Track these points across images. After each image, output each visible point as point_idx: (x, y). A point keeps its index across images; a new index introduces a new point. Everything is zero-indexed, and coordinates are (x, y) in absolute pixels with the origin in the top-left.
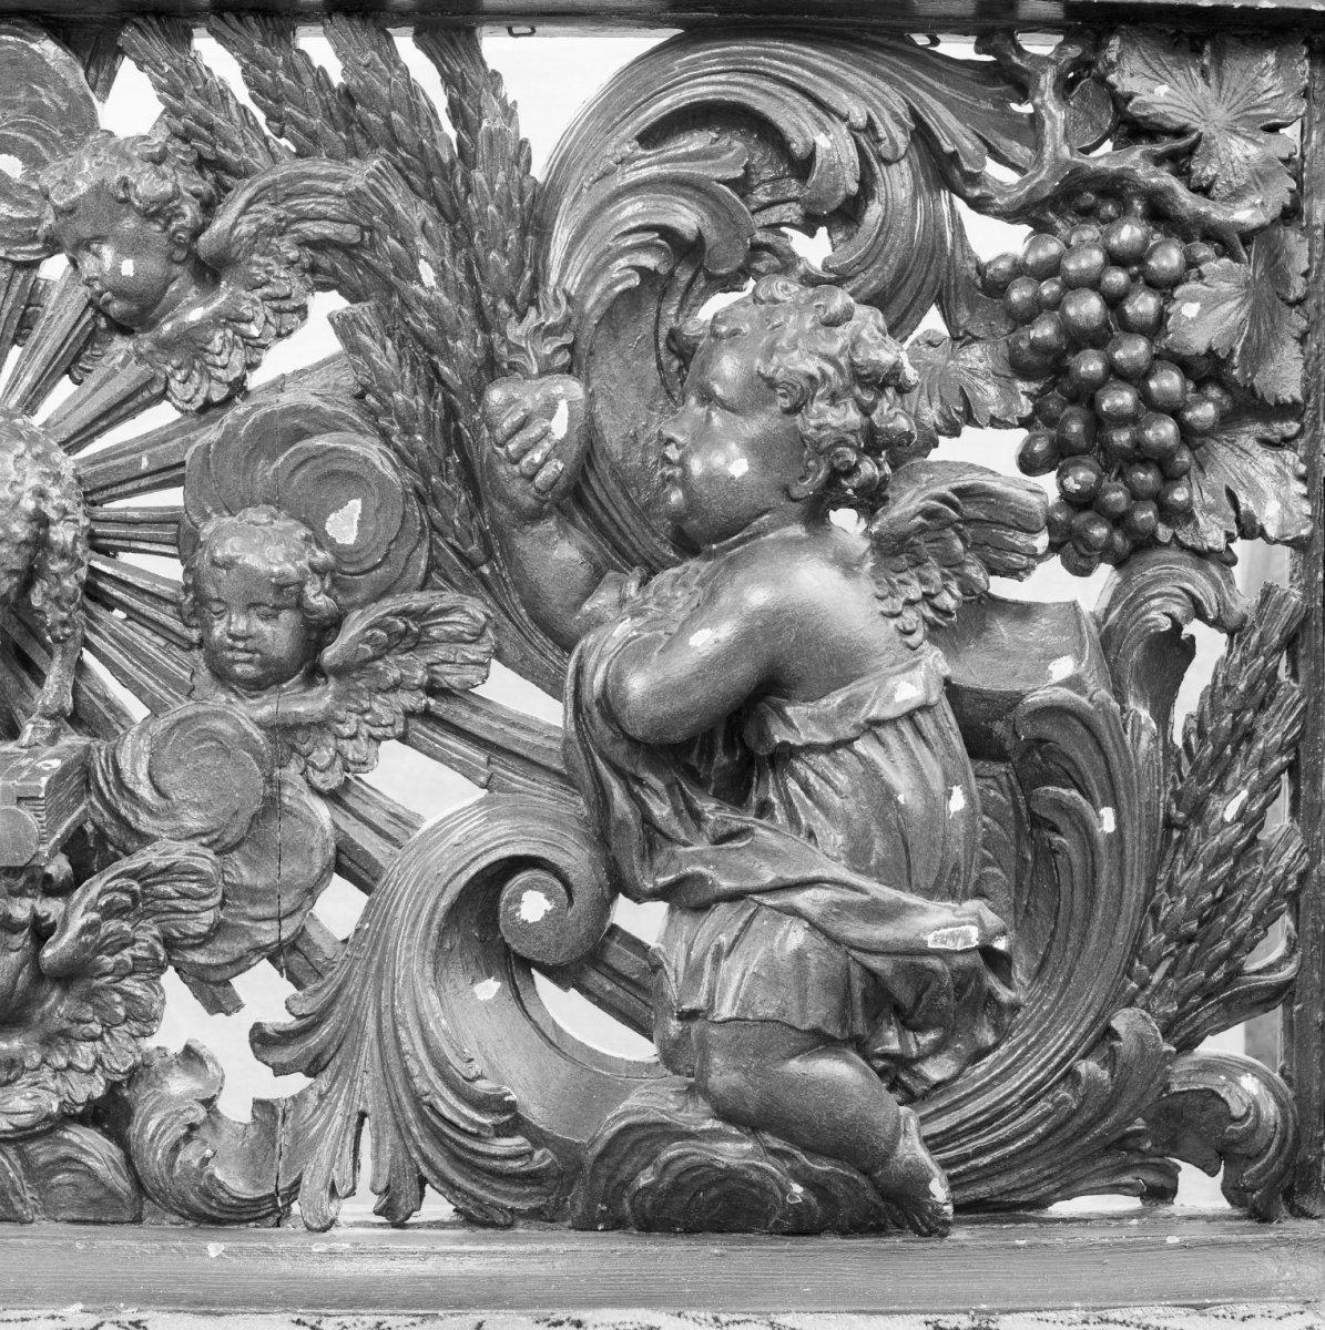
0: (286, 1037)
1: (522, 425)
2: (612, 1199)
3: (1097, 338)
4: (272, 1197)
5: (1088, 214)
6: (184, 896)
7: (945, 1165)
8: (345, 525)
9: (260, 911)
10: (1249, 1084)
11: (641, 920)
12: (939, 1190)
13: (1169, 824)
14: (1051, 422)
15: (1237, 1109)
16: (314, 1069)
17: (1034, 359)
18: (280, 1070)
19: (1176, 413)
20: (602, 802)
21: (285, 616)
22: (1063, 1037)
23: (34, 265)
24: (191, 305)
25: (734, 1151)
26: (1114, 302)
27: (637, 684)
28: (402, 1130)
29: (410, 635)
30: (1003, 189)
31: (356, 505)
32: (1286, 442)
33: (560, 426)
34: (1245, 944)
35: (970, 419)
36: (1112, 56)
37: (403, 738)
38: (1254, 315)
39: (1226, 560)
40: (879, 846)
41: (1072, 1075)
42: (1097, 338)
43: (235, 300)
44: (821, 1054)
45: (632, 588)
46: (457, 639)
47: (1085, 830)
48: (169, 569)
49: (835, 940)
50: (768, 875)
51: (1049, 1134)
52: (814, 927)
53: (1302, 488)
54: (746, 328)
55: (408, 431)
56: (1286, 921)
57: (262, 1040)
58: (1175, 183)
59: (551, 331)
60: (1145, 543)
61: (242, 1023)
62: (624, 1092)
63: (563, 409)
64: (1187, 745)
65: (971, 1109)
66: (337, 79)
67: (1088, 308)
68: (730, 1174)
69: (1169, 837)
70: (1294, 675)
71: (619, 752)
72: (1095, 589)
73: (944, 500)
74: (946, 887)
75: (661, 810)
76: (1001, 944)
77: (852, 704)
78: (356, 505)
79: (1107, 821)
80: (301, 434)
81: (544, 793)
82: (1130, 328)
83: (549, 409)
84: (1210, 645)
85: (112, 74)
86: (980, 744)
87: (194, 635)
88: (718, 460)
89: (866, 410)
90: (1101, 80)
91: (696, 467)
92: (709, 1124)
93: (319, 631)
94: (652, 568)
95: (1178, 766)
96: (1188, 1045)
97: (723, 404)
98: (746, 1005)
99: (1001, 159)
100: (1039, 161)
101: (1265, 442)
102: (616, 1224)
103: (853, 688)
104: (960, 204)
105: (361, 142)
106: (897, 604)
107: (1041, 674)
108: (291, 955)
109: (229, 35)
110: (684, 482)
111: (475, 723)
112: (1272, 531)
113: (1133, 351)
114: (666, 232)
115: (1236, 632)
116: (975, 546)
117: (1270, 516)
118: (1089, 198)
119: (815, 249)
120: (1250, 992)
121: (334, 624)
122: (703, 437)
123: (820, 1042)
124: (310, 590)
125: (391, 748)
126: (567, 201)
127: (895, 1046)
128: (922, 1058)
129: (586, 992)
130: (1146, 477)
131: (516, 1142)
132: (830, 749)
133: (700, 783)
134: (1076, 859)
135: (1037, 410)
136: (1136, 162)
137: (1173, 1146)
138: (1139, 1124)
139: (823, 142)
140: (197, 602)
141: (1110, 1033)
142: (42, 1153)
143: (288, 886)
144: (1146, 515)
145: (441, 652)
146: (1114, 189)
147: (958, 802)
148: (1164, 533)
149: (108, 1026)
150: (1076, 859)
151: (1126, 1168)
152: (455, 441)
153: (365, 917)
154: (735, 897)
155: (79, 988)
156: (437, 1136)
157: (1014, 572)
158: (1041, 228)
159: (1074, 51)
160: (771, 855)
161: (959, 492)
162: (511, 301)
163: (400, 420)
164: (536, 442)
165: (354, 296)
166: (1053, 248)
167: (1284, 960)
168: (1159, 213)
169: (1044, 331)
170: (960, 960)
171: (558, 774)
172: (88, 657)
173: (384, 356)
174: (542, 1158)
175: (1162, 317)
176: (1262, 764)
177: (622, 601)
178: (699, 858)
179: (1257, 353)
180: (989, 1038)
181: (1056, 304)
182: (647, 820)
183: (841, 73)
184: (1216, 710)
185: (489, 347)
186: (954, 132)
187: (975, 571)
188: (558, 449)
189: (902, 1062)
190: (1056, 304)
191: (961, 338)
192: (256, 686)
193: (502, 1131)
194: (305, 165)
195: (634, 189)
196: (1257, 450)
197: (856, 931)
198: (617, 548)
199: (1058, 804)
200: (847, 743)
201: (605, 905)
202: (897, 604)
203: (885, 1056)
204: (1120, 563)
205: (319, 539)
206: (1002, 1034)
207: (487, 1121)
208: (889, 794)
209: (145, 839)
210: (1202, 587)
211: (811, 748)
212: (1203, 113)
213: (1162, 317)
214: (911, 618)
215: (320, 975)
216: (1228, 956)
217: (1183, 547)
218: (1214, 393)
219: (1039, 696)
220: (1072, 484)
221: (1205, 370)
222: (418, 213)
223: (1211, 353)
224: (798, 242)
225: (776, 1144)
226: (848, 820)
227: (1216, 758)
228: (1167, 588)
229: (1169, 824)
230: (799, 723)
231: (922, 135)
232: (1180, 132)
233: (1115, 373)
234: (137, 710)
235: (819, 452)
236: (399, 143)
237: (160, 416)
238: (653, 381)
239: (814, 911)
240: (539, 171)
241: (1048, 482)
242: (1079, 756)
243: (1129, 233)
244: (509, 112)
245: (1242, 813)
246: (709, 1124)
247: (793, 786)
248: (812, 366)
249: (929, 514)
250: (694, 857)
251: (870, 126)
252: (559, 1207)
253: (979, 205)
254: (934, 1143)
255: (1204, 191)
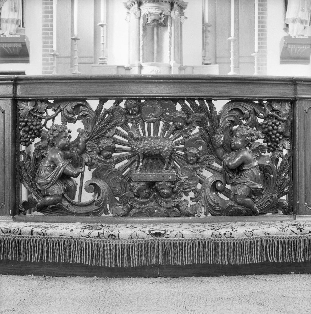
0: (194, 198)
1: (219, 139)
2: (227, 213)
3: (271, 131)
4: (194, 214)
5: (269, 118)
6: (185, 184)
7: (259, 209)
8: (200, 149)
9: (192, 186)
10: (285, 201)
11: (228, 187)
12: (258, 211)
13: (277, 177)
14: (266, 138)
15: (284, 204)
16: (197, 202)
17: (265, 132)
18: (193, 202)
19: (278, 138)
20: (226, 175)
21: (196, 157)
22: (268, 197)
23: (169, 123)
24: (186, 127)
25: (239, 208)
26: (273, 127)
27: (230, 164)
28: (207, 207)
29: (207, 159)
30: (262, 116)
31: (202, 146)
32: (288, 140)
33: (222, 139)
34: (284, 188)
35: (259, 138)
36: (272, 103)
37: (205, 169)
38: (285, 128)
39: (282, 151)
40: (253, 178)
41: (269, 201)
42: (271, 131)
43: (190, 127)
44: (248, 198)
45: (228, 154)
46: (212, 159)
47: (270, 177)
48: (183, 153)
49: (249, 187)
50: (243, 181)
51: (267, 206)
52: (247, 186)
53: (289, 144)
54: (240, 130)
55: (206, 139)
56: (288, 186)
57: (191, 199)
58: (278, 115)
59: (221, 130)
60: (275, 150)
61: (189, 197)
62: (228, 203)
63: (222, 137)
64: (279, 169)
65: (260, 204)
66: (199, 105)
67: (271, 128)
68: (239, 210)
69: (277, 178)
70: (289, 162)
71: (228, 170)
72: (270, 154)
73: (258, 146)
74: (259, 183)
75: (231, 176)
76: (263, 188)
77: (251, 165)
78: (202, 146)
79: (272, 176)
80: (196, 140)
81: (219, 174)
82: (274, 129)
83: (221, 137)
84: (281, 159)
85: (176, 104)
86: (261, 170)
87: (185, 159)
88: (237, 142)
89: (251, 138)
90: (271, 106)
91: (235, 143)
92: (237, 205)
93: (198, 159)
94: (229, 153)
95: (278, 171)
96: (279, 198)
97: (238, 137)
98: (241, 193)
99: (262, 113)
100: (265, 113)
101: (286, 140)
102: (227, 215)
103: (251, 164)
104: (257, 117)
105: (201, 111)
106: (253, 156)
107: (266, 162)
108: (195, 191)
109: (190, 101)
110: (234, 144)
111: (213, 168)
112: (287, 149)
113: (275, 132)
114: (231, 120)
115: (283, 158)
116: (261, 150)
117: (287, 147)
118: (270, 117)
119: (244, 122)
120: (285, 193)
121: (199, 158)
122: (236, 140)
123: (248, 197)
124: (198, 155)
125: (204, 170)
126: (221, 117)
127: (254, 198)
128: (255, 199)
129: (223, 194)
130: (275, 143)
131: (218, 208)
132: (248, 169)
133: (234, 173)
134: (269, 180)
135: (265, 137)
136: (274, 113)
137: (278, 208)
138: (275, 205)
139: (246, 112)
140: (186, 156)
141: (272, 197)
142: (171, 210)
143: (195, 184)
144: (275, 147)
145: (210, 161)
146: (272, 116)
147: (259, 175)
148: (277, 149)
149: (178, 197)
150: (269, 180)
151: (273, 210)
152: (210, 140)
153: (202, 187)
154: (239, 184)
155: (176, 194)
156: (211, 207)
157: (264, 153)
158: (265, 120)
159: (268, 103)
160: (243, 179)
161: (260, 145)
162: (216, 127)
163: (206, 138)
164: (220, 141)
165: (200, 126)
166: (267, 122)
167: (288, 190)
168: (276, 118)
169: (266, 130)
170: (260, 189)
171: (220, 172)
172: (174, 162)
173: (204, 132)
174: (221, 209)
175: (277, 129)
176: (286, 171)
177: (227, 156)
178: (235, 180)
179: (286, 132)
180: (261, 197)
181: (268, 127)
182: (230, 177)
183: (176, 52)
184: (282, 166)
185: (214, 131)
186: (257, 111)
187: (261, 153)
188: (222, 141)
189: (254, 199)
190: (268, 127)
191: (257, 130)
192: (192, 164)
193: (217, 206)
194: (196, 114)
195: (227, 117)
196: (285, 141)
197: (251, 186)
198: (225, 150)
199: (267, 175)
200: (250, 169)
201: (225, 185)
202: (253, 156)
203: (252, 199)
204: (272, 152)
205: (198, 150)
206: (262, 197)
207: (216, 205)
208: (254, 174)
209: (181, 179)
210: (280, 153)
211: (247, 169)
212: (280, 109)
213: (277, 129)
214: (255, 157)
215: (197, 192)
216: (283, 189)
217: (278, 150)
218: (281, 135)
219: (266, 164)
220: (269, 144)
221: (281, 133)
222: (207, 118)
223: (282, 132)
224: (242, 121)
225: (243, 207)
226: (250, 176)
227: (282, 170)
228: (278, 154)
229: (277, 177)
230: (245, 167)
231: (255, 111)
232: (278, 111)
233: (273, 134)
234: (179, 167)
235: (247, 141)
236: (205, 111)
237: (181, 138)
238: (229, 134)
239: (247, 185)
240: (218, 114)
241: (266, 144)
242: (269, 170)
243: (274, 121)
244: (215, 108)
245: (284, 176)
246: (237, 205)
247: (244, 173)
248: (247, 134)
249: (257, 147)
250: (234, 180)
251: (250, 110)
252: (222, 214)
253: (259, 117)
254: (257, 207)
255: (280, 116)
